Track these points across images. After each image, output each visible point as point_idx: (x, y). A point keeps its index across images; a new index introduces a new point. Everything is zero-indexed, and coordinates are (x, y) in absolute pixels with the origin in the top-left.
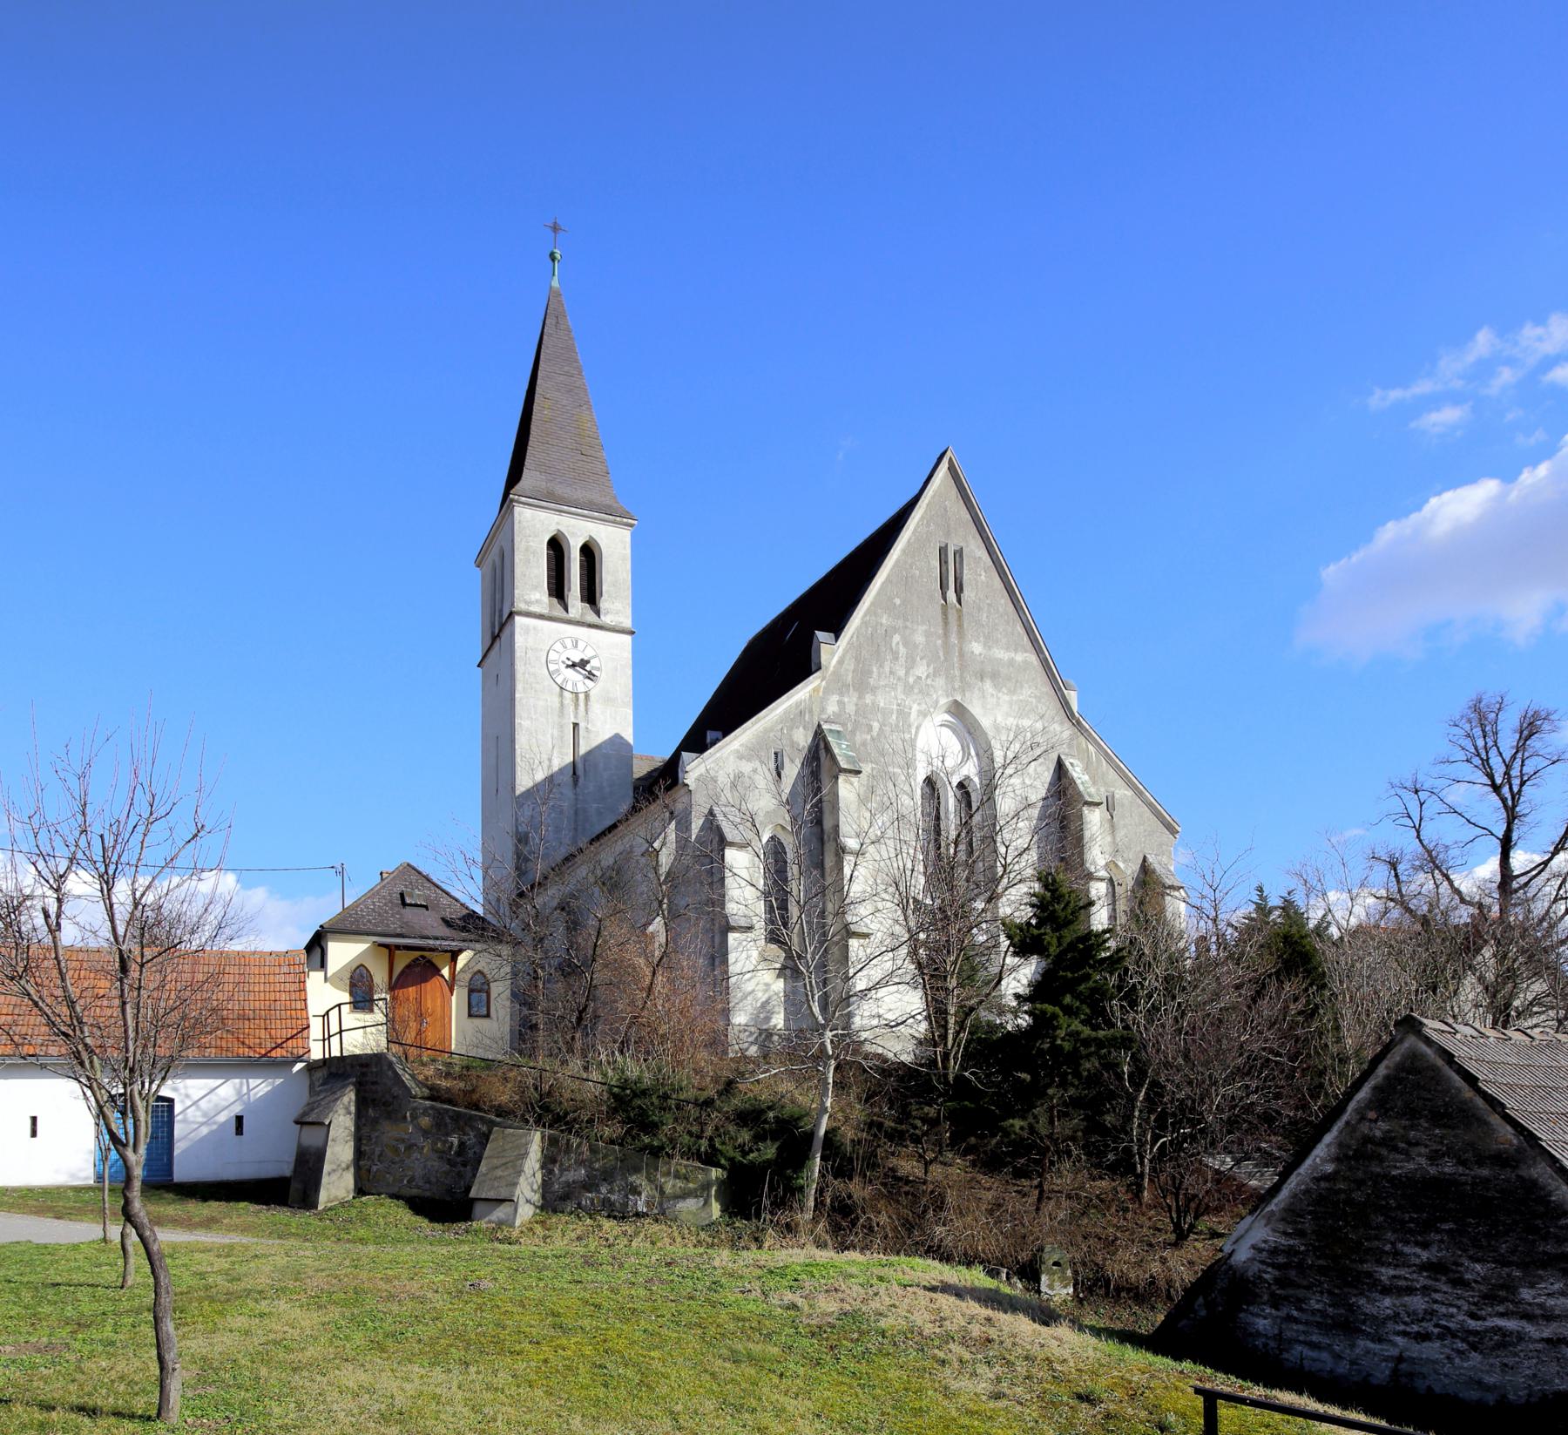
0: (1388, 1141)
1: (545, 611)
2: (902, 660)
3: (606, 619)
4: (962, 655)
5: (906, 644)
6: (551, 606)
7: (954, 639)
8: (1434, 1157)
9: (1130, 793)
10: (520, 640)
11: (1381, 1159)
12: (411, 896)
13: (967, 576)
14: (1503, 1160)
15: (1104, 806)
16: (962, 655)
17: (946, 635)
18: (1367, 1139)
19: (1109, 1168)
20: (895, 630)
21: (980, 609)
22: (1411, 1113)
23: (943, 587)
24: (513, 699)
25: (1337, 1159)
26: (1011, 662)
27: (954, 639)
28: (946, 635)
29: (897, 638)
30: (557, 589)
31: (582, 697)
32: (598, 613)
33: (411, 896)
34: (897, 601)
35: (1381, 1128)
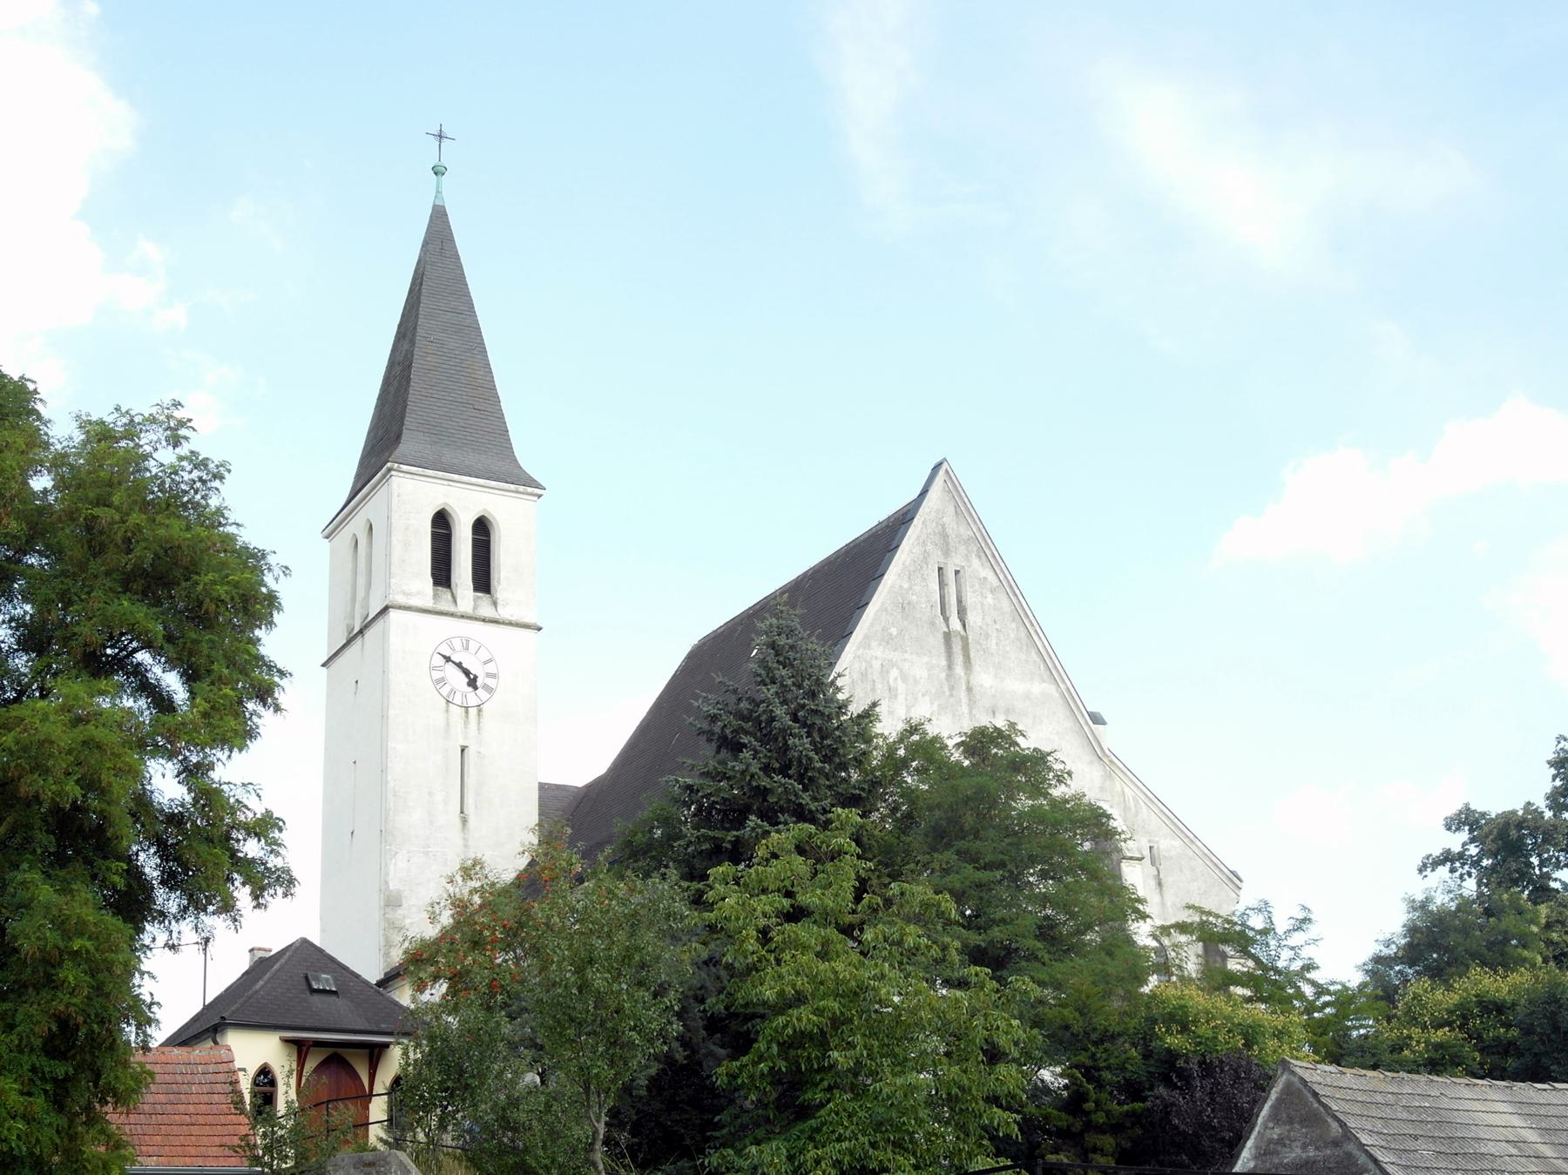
0: (1280, 1141)
1: (428, 603)
2: (901, 698)
3: (504, 613)
4: (969, 689)
5: (904, 678)
6: (435, 596)
7: (959, 670)
8: (1304, 1147)
9: (1177, 843)
10: (395, 639)
11: (1278, 1153)
12: (318, 980)
13: (970, 599)
14: (1336, 1143)
15: (1147, 861)
16: (969, 689)
17: (950, 667)
18: (1270, 1141)
19: (904, 763)
20: (893, 664)
21: (987, 636)
22: (1290, 1121)
23: (943, 611)
24: (384, 717)
25: (1256, 1158)
26: (1027, 696)
27: (959, 670)
28: (950, 667)
29: (894, 673)
30: (442, 574)
31: (473, 712)
32: (495, 604)
33: (318, 980)
34: (894, 631)
35: (1276, 1133)
